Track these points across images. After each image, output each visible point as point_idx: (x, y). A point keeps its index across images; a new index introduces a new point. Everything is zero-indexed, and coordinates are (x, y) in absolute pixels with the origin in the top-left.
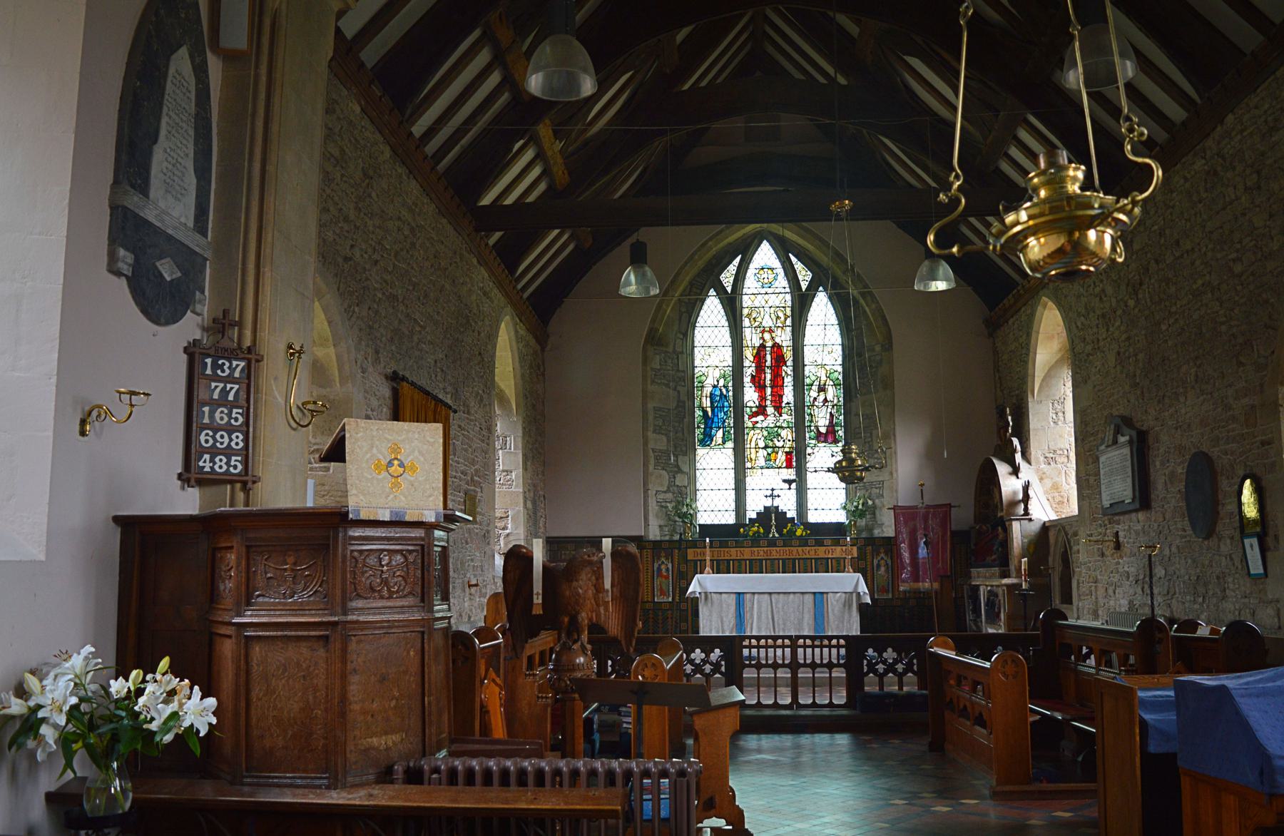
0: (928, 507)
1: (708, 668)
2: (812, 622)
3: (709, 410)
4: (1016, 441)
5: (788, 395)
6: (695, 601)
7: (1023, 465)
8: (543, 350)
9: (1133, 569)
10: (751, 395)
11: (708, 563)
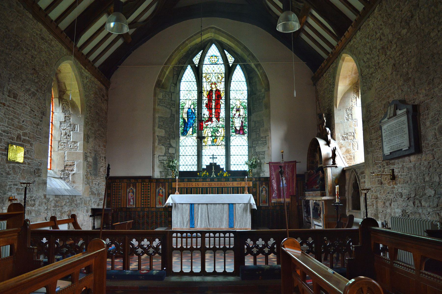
0: (285, 162)
1: (151, 250)
2: (227, 218)
3: (186, 119)
4: (328, 129)
5: (223, 114)
7: (332, 141)
8: (107, 88)
9: (405, 191)
10: (205, 112)
11: (177, 189)
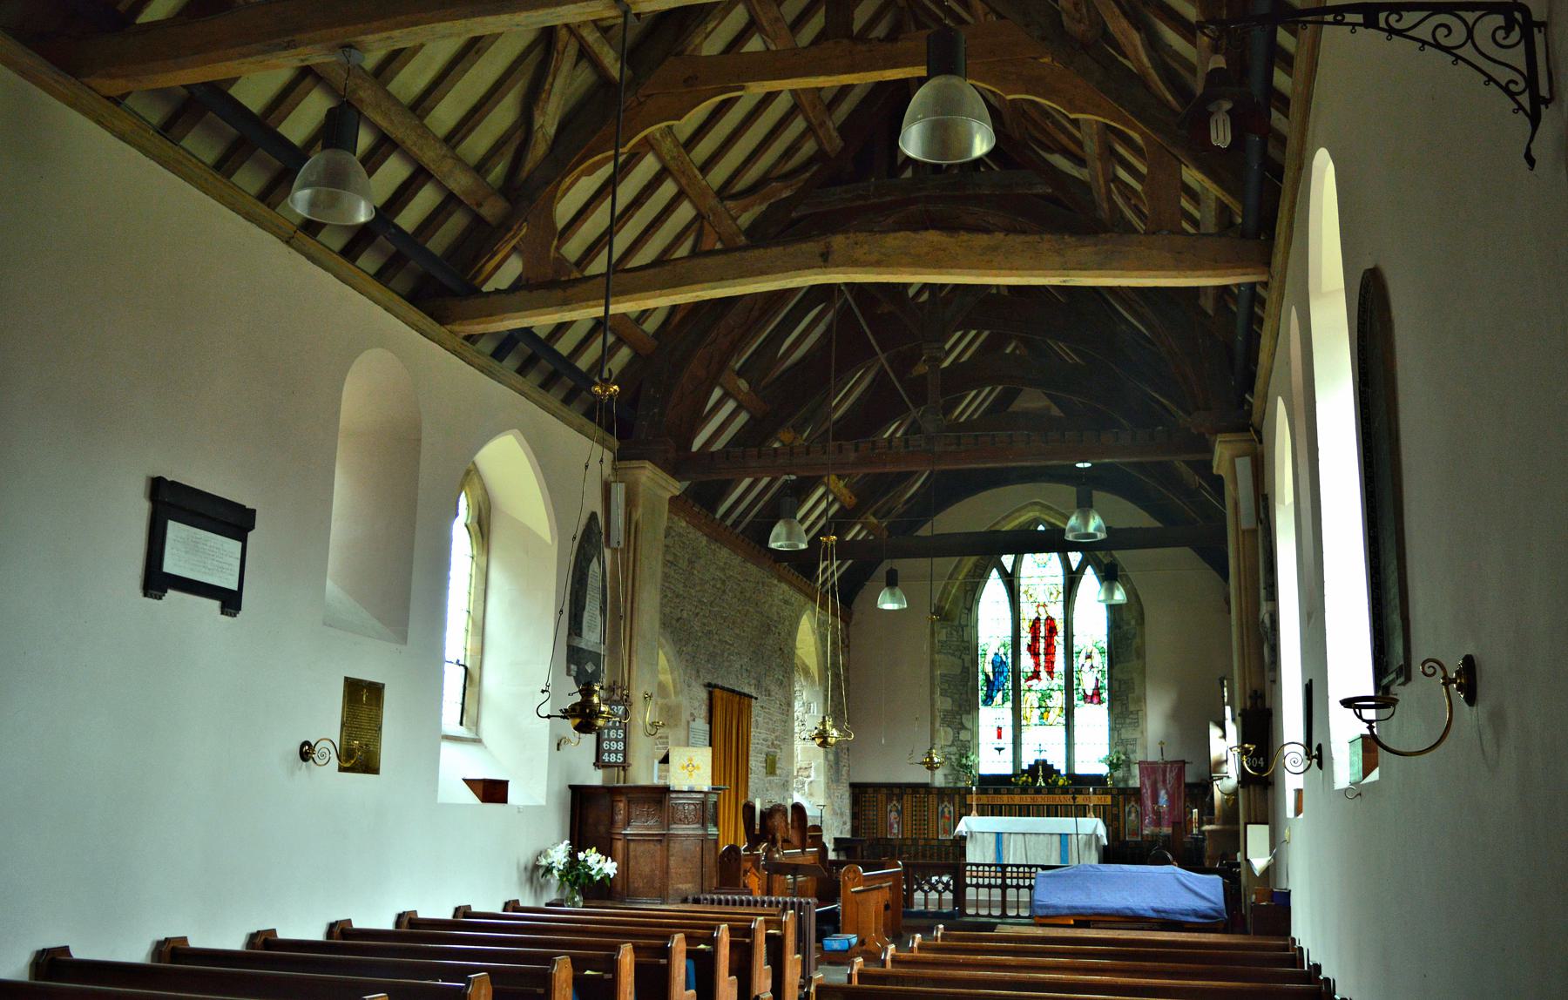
6: (964, 838)
10: (1027, 663)
